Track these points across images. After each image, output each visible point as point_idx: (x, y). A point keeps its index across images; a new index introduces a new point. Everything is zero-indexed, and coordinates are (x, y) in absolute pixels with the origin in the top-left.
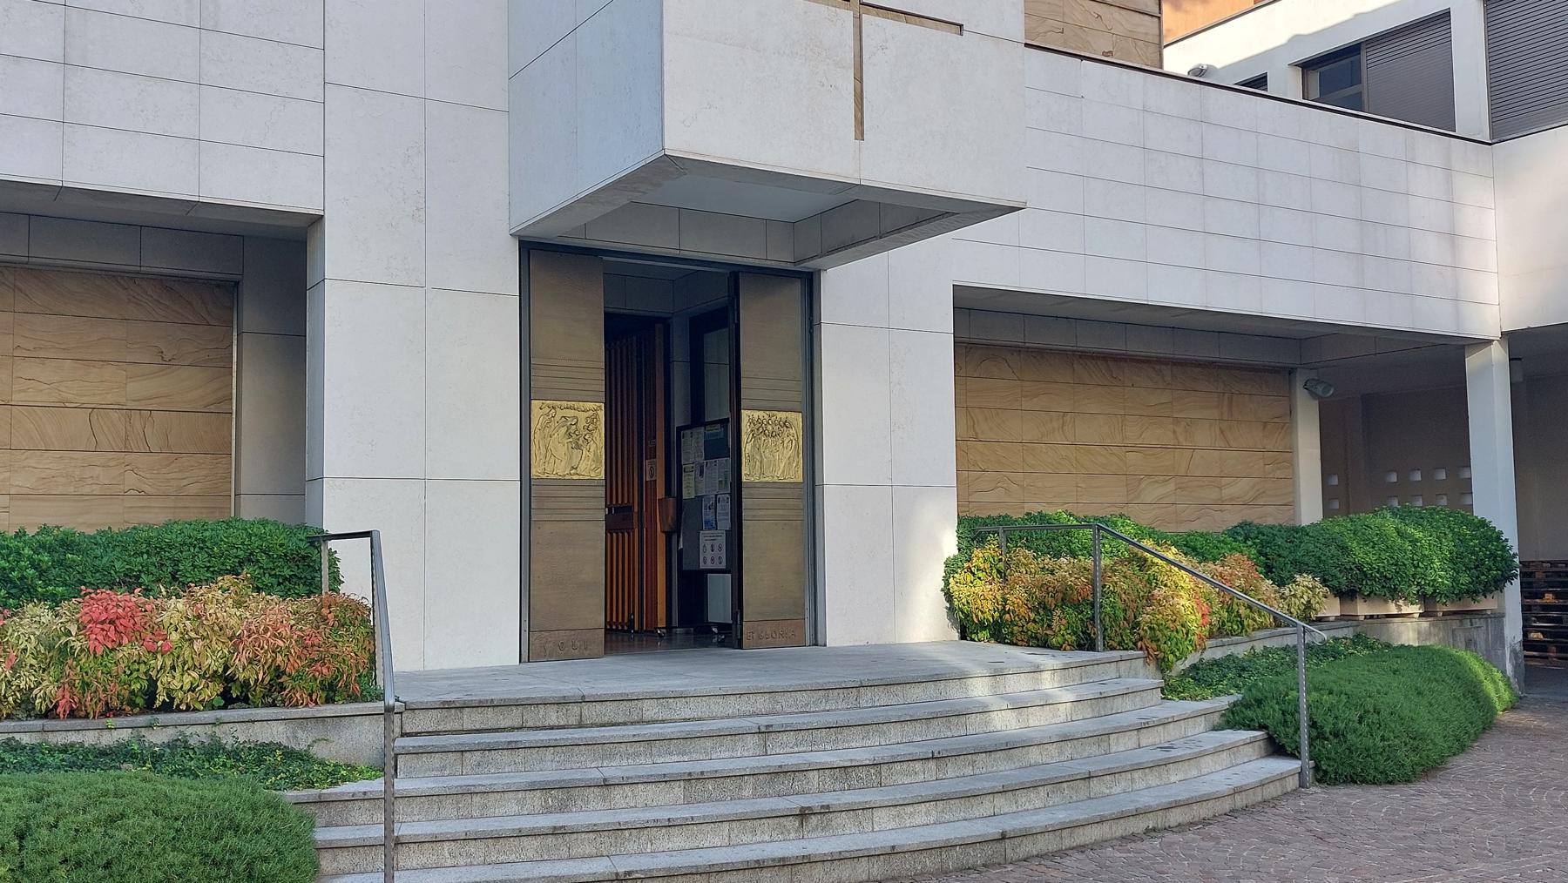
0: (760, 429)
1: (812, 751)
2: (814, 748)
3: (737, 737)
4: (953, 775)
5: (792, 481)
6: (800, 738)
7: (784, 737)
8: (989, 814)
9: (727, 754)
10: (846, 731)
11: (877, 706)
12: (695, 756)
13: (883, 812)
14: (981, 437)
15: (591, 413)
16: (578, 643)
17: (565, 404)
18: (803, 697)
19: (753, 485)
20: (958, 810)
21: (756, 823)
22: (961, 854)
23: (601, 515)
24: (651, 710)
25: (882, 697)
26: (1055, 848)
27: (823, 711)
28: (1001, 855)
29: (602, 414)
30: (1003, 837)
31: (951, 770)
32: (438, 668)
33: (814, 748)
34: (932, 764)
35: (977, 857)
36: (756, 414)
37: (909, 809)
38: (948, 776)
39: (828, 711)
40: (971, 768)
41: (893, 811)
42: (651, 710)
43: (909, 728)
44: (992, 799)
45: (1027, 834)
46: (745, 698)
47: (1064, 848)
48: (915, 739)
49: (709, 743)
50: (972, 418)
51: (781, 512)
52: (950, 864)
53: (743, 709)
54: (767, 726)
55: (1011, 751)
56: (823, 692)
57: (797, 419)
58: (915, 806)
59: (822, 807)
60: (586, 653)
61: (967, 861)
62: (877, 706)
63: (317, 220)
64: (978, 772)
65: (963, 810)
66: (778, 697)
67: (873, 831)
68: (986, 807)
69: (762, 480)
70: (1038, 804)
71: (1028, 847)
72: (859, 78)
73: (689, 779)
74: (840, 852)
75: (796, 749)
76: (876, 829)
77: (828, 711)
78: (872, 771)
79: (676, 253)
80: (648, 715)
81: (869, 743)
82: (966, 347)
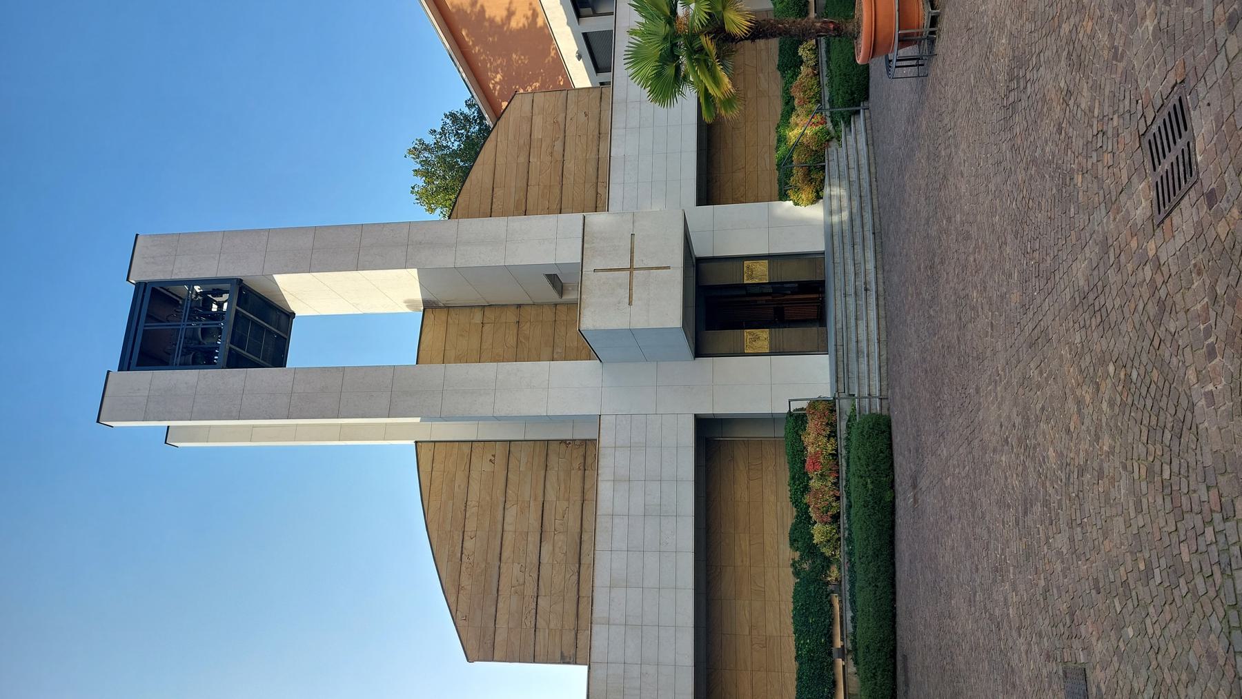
0: (751, 277)
7: (847, 289)
15: (747, 333)
29: (748, 330)
30: (874, 233)
34: (855, 247)
41: (866, 263)
49: (848, 311)
57: (746, 263)
72: (652, 268)
73: (856, 319)
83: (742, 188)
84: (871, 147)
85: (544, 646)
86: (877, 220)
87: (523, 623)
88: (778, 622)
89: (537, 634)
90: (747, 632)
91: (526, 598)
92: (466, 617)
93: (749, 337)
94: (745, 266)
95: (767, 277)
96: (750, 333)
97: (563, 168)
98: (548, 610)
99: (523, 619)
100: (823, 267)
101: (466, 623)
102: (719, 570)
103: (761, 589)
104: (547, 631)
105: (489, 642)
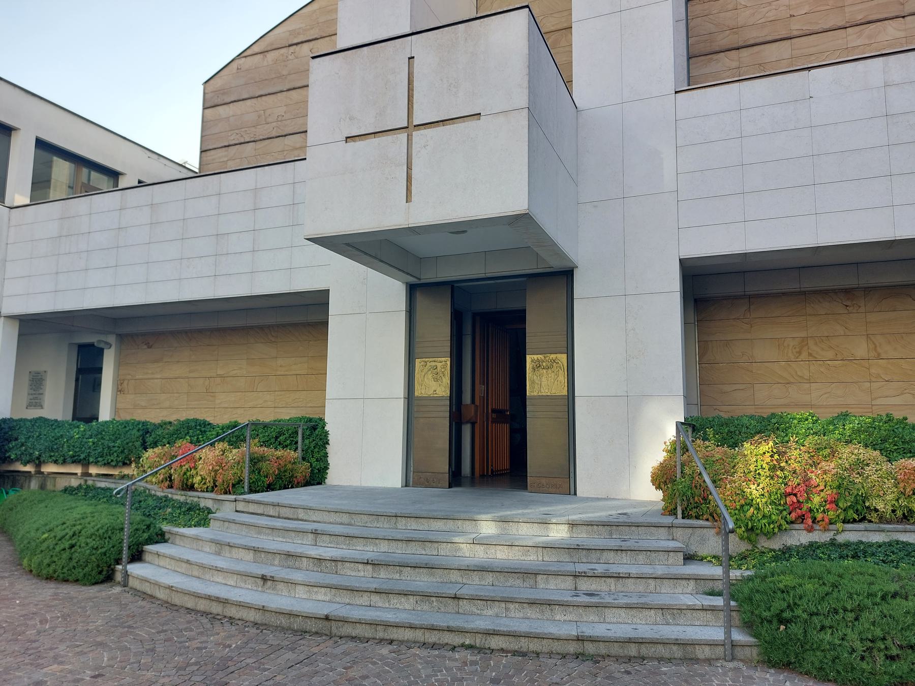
0: (538, 366)
1: (336, 548)
2: (338, 546)
3: (305, 534)
4: (384, 577)
5: (560, 394)
6: (332, 539)
7: (324, 537)
8: (366, 604)
9: (300, 542)
10: (355, 540)
11: (409, 530)
12: (288, 540)
13: (301, 588)
14: (884, 356)
15: (444, 364)
16: (435, 480)
17: (431, 359)
18: (365, 518)
19: (534, 398)
20: (346, 598)
21: (247, 578)
22: (302, 621)
23: (448, 414)
24: (301, 514)
25: (413, 524)
26: (370, 635)
27: (376, 527)
28: (328, 630)
29: (449, 363)
30: (327, 618)
31: (383, 574)
32: (348, 484)
33: (338, 546)
34: (369, 567)
35: (312, 626)
36: (535, 357)
37: (315, 589)
38: (381, 576)
39: (378, 528)
40: (398, 575)
41: (307, 588)
42: (301, 514)
43: (394, 544)
44: (369, 595)
45: (345, 621)
46: (338, 514)
47: (378, 637)
48: (397, 551)
49: (293, 534)
50: (873, 342)
51: (552, 413)
52: (295, 625)
53: (337, 520)
54: (315, 530)
55: (433, 570)
56: (376, 517)
57: (563, 358)
58: (319, 588)
59: (271, 576)
60: (439, 485)
61: (306, 626)
62: (409, 530)
63: (326, 292)
64: (404, 578)
65: (348, 597)
66: (353, 516)
67: (295, 597)
68: (364, 599)
69: (540, 394)
70: (407, 607)
71: (348, 630)
72: (409, 168)
73: (256, 550)
74: (240, 602)
75: (329, 545)
76: (297, 596)
77: (378, 528)
78: (333, 564)
79: (483, 276)
80: (300, 516)
81: (367, 549)
82: (864, 291)
83: (830, 354)
84: (572, 648)
85: (213, 159)
86: (358, 631)
87: (232, 132)
88: (226, 406)
89: (224, 149)
90: (220, 372)
91: (253, 129)
92: (240, 69)
93: (439, 365)
94: (559, 356)
95: (535, 394)
96: (444, 367)
97: (886, 19)
98: (243, 157)
99: (236, 131)
100: (550, 490)
101: (235, 71)
102: (273, 340)
103: (255, 388)
104: (226, 159)
105: (219, 100)
